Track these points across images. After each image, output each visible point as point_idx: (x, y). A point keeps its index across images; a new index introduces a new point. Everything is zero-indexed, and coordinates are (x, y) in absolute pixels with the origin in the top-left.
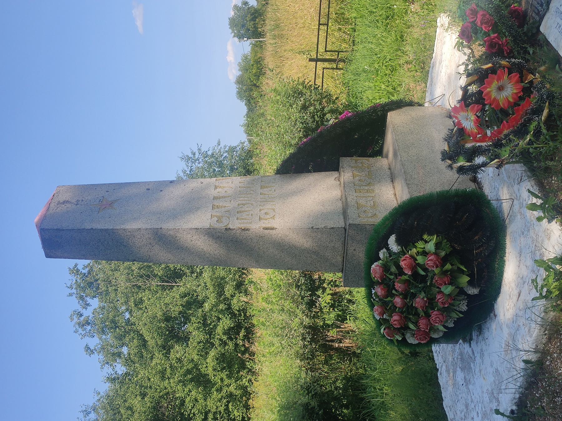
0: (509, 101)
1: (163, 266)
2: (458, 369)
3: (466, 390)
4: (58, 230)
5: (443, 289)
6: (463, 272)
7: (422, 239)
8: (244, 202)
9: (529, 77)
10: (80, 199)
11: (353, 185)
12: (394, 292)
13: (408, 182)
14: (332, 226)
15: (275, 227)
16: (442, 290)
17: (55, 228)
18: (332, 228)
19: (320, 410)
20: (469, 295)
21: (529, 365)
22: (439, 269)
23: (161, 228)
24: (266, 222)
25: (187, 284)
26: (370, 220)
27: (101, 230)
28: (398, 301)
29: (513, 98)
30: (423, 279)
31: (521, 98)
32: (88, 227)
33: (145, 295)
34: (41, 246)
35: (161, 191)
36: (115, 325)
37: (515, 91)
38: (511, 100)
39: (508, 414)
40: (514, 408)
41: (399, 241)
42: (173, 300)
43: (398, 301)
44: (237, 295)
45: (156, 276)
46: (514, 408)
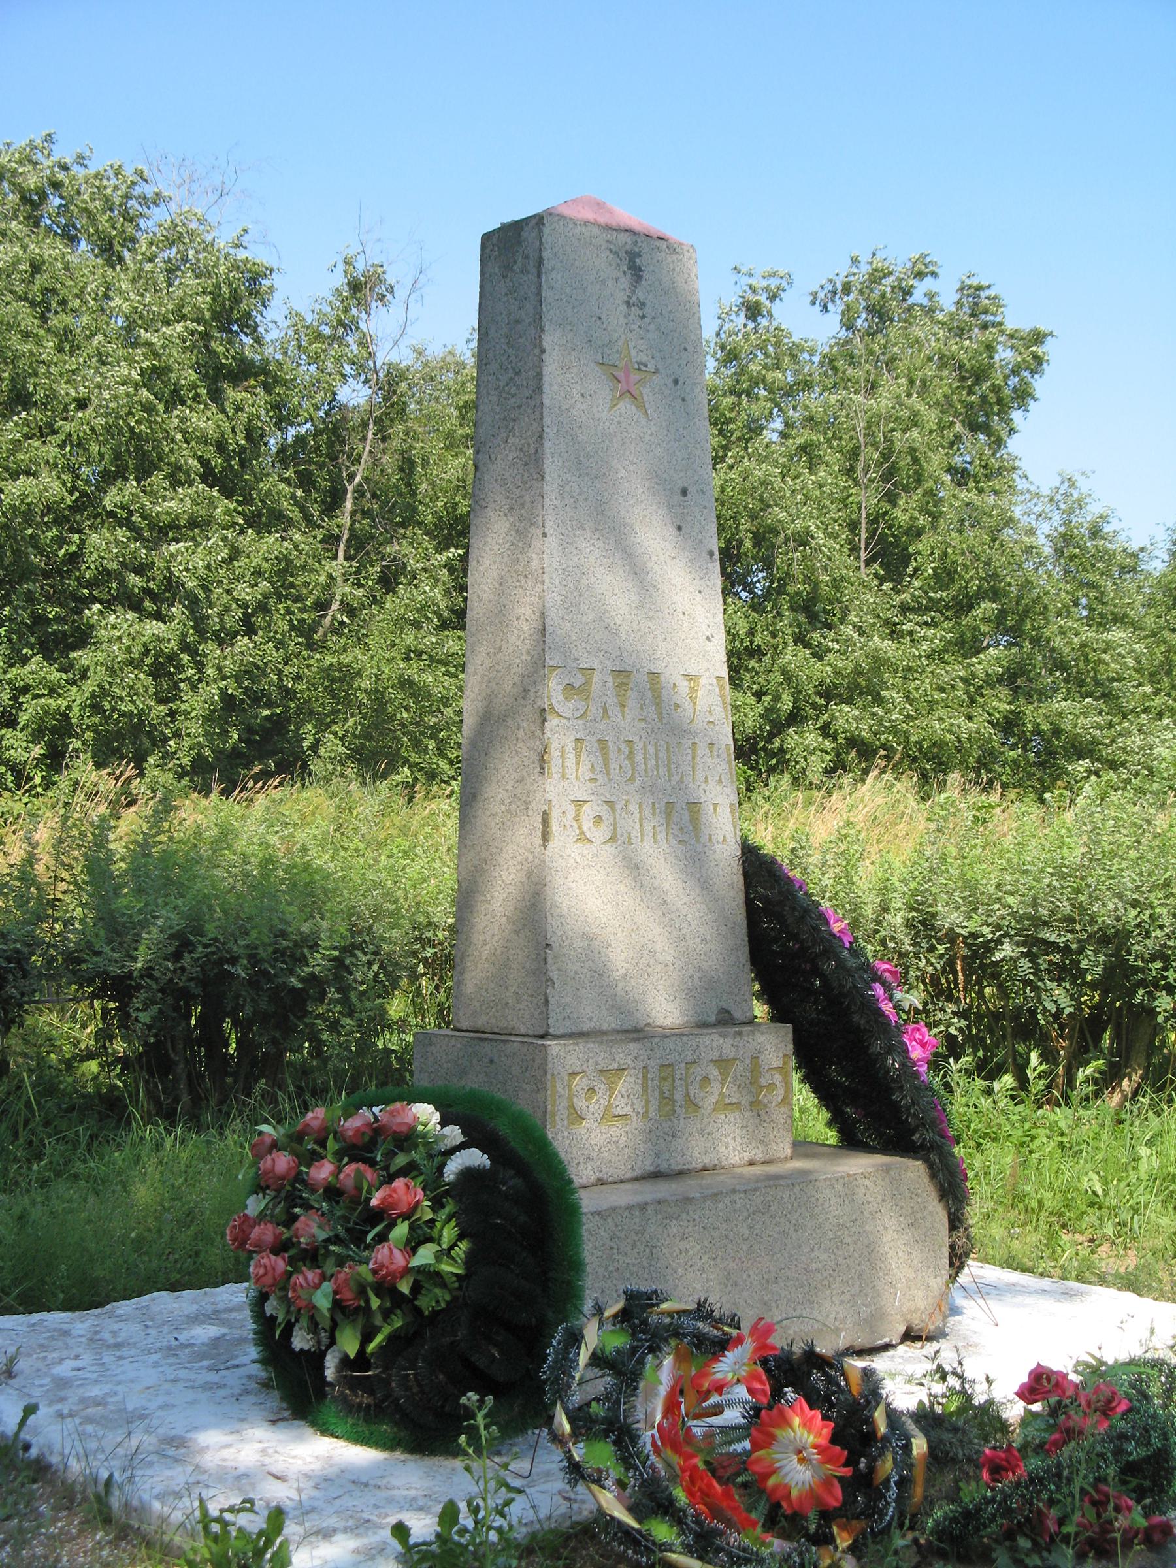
0: (767, 1476)
1: (922, 521)
2: (224, 1330)
3: (158, 1345)
4: (540, 262)
5: (327, 1287)
6: (367, 1338)
7: (461, 1237)
8: (639, 758)
9: (845, 1535)
10: (647, 311)
11: (690, 1058)
12: (346, 1160)
13: (650, 1209)
14: (551, 1000)
15: (551, 845)
16: (326, 1284)
17: (545, 255)
18: (547, 1001)
19: (302, 980)
20: (321, 1356)
21: (101, 1488)
22: (370, 1278)
23: (544, 535)
24: (569, 819)
25: (866, 595)
26: (562, 1104)
27: (539, 376)
28: (323, 1172)
29: (776, 1487)
30: (358, 1237)
31: (775, 1507)
32: (548, 341)
33: (827, 476)
34: (508, 220)
35: (679, 528)
36: (742, 389)
37: (794, 1493)
38: (771, 1482)
39: (22, 1435)
40: (34, 1452)
41: (468, 1174)
42: (834, 558)
43: (323, 1172)
44: (828, 745)
45: (891, 498)
46: (34, 1452)
